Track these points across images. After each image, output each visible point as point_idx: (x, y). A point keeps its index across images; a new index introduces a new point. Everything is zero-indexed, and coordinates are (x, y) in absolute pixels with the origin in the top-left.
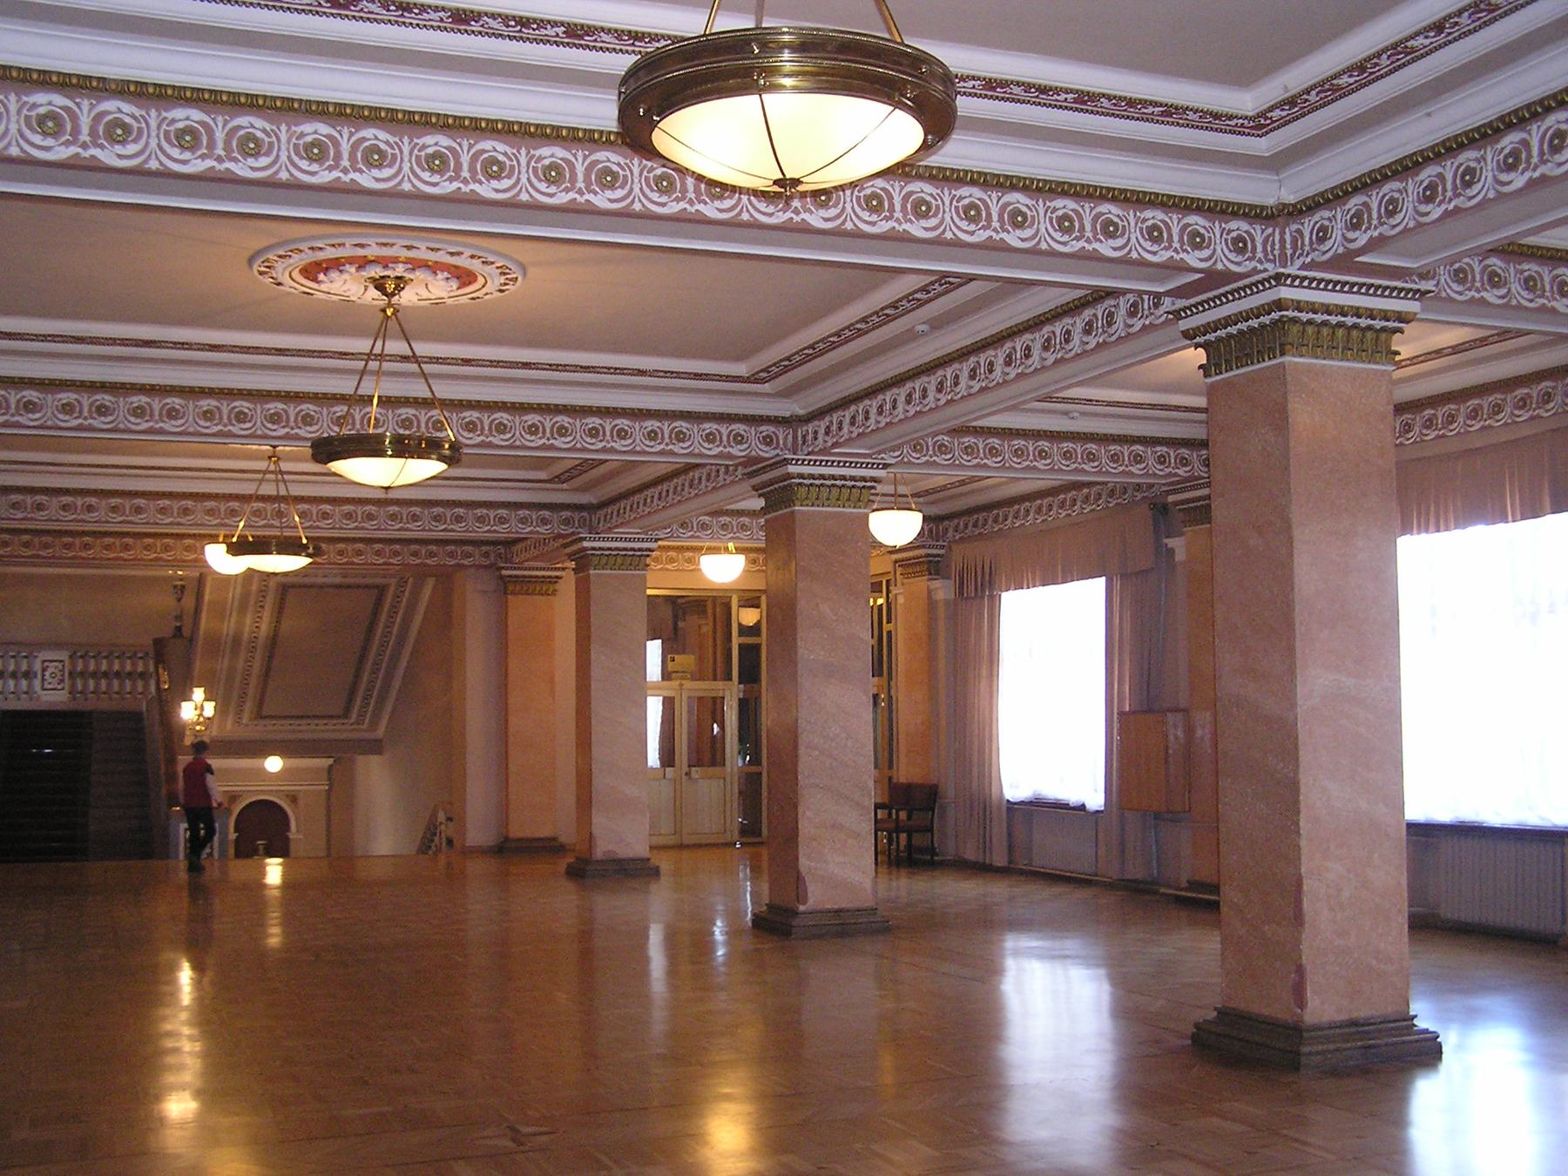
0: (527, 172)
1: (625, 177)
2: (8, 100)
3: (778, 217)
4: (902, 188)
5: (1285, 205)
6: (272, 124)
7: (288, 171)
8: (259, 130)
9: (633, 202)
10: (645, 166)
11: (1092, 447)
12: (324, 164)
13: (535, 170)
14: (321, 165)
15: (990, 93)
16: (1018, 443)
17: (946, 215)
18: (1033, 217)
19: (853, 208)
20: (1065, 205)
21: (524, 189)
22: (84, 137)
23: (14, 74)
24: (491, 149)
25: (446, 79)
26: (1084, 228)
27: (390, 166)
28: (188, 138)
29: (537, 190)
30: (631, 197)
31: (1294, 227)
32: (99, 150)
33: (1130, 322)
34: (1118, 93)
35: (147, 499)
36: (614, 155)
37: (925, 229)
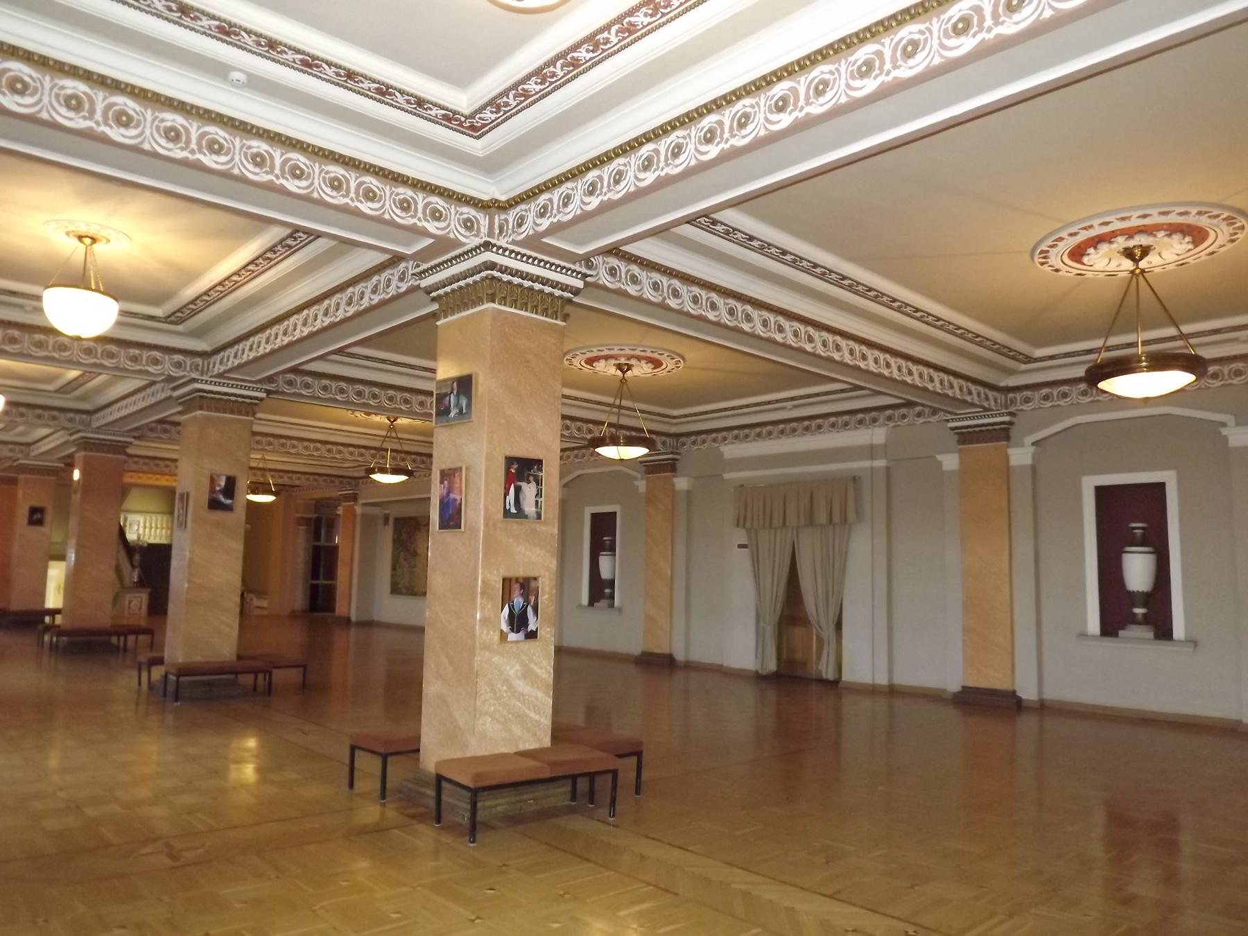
0: (319, 179)
1: (381, 196)
2: (45, 80)
3: (78, 123)
4: (424, 199)
5: (496, 200)
6: (231, 135)
7: (240, 169)
8: (221, 137)
9: (384, 213)
10: (393, 192)
11: (376, 390)
12: (340, 192)
13: (324, 178)
14: (261, 169)
15: (378, 97)
16: (391, 393)
17: (386, 202)
18: (596, 265)
19: (152, 134)
20: (337, 171)
21: (315, 190)
22: (194, 146)
23: (36, 58)
24: (369, 182)
25: (458, 169)
26: (480, 230)
27: (32, 95)
28: (75, 103)
29: (325, 193)
30: (312, 188)
31: (503, 217)
32: (285, 180)
33: (400, 285)
34: (260, 30)
35: (162, 353)
36: (375, 181)
37: (437, 228)
